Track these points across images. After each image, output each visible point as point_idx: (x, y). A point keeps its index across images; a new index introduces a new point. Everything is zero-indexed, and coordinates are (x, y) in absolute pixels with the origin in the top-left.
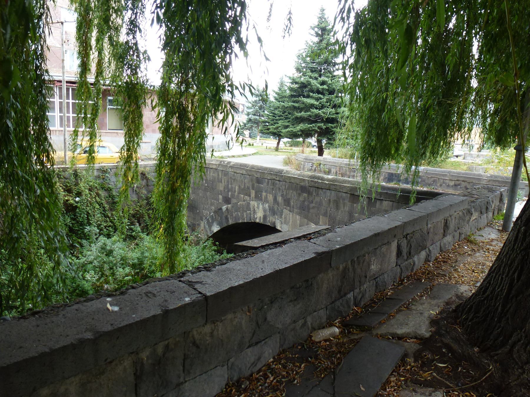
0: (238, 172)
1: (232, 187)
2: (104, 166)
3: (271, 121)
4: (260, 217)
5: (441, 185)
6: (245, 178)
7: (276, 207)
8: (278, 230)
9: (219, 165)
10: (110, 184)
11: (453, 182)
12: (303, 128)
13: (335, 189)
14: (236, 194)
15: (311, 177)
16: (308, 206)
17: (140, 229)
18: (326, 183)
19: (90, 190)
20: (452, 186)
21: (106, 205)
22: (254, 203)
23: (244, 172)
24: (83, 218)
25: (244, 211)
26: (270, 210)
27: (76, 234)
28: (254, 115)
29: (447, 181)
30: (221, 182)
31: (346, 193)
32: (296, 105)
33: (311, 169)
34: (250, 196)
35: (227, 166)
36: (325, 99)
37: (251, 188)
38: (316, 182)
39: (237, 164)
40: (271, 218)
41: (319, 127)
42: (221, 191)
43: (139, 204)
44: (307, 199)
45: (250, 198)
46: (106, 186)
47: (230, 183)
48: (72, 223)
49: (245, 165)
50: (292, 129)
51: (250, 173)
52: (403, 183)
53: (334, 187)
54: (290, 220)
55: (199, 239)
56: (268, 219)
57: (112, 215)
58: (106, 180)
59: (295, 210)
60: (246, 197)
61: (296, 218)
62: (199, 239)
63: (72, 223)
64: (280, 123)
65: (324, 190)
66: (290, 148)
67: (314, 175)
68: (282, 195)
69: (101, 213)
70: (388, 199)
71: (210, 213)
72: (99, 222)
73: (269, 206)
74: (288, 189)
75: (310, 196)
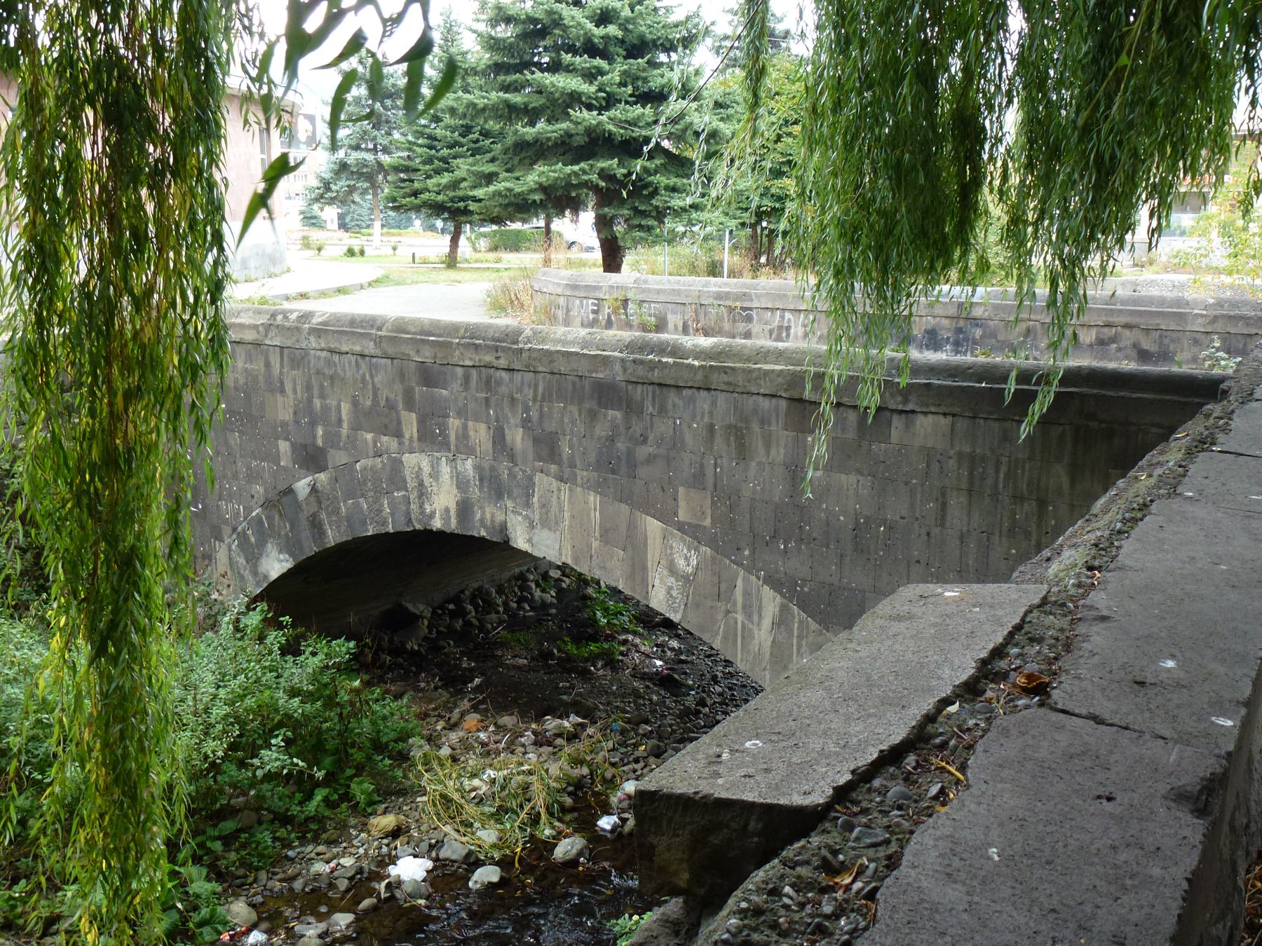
0: (345, 348)
1: (325, 408)
3: (424, 163)
4: (447, 510)
6: (373, 370)
7: (504, 467)
8: (519, 551)
9: (268, 327)
11: (1093, 332)
12: (548, 177)
13: (729, 384)
14: (345, 430)
15: (631, 347)
16: (630, 454)
18: (690, 366)
20: (1091, 345)
22: (416, 462)
23: (370, 348)
25: (379, 492)
26: (481, 480)
28: (357, 148)
30: (283, 391)
32: (516, 98)
34: (398, 434)
35: (298, 329)
36: (616, 73)
37: (401, 406)
38: (652, 366)
39: (336, 319)
40: (488, 510)
41: (603, 174)
42: (284, 424)
44: (622, 429)
47: (316, 392)
49: (373, 322)
50: (508, 185)
52: (920, 347)
53: (725, 378)
54: (561, 510)
55: (215, 609)
56: (478, 516)
59: (581, 475)
60: (385, 439)
61: (586, 503)
62: (215, 609)
64: (463, 167)
65: (686, 392)
66: (491, 256)
67: (643, 338)
68: (526, 423)
70: (933, 409)
71: (248, 510)
73: (477, 468)
74: (547, 397)
75: (634, 418)
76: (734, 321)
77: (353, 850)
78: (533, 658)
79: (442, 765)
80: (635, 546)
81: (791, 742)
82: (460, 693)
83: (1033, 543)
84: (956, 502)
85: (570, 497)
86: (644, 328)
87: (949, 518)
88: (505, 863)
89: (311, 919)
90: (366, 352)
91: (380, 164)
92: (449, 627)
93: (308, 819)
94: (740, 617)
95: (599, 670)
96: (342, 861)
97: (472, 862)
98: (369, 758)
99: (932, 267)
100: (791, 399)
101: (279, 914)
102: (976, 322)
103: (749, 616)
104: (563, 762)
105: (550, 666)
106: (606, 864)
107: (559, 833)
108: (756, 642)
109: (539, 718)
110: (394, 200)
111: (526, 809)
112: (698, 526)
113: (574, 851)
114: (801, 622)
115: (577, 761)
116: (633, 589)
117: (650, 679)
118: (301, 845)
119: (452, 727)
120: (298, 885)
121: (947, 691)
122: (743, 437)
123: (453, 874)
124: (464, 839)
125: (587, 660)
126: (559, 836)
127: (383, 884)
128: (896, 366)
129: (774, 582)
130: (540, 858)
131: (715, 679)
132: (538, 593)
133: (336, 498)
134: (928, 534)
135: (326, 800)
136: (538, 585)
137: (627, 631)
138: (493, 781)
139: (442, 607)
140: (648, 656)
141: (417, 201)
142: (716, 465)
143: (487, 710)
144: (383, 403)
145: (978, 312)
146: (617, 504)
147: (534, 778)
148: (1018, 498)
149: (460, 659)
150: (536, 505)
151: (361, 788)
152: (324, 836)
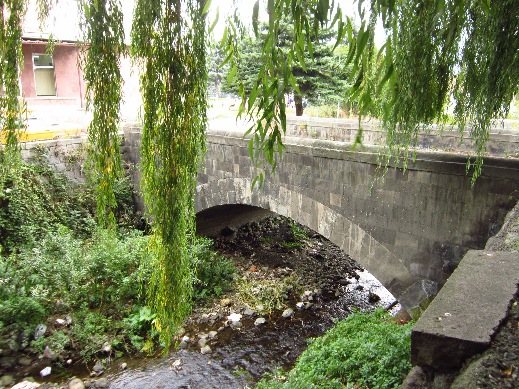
0: (215, 142)
1: (208, 162)
2: (40, 144)
4: (248, 198)
5: (459, 146)
6: (225, 149)
10: (49, 167)
13: (350, 158)
14: (214, 169)
15: (315, 144)
16: (313, 181)
17: (94, 221)
19: (23, 177)
20: (473, 146)
21: (47, 195)
22: (238, 181)
23: (224, 142)
24: (18, 214)
25: (225, 191)
27: (10, 236)
29: (466, 141)
31: (366, 163)
33: (295, 133)
34: (232, 171)
38: (323, 151)
40: (263, 198)
43: (89, 189)
45: (233, 174)
46: (45, 170)
48: (4, 223)
51: (231, 143)
53: (348, 156)
54: (288, 199)
56: (259, 200)
57: (56, 206)
58: (44, 162)
59: (296, 187)
60: (228, 173)
63: (4, 223)
69: (41, 205)
70: (424, 170)
72: (40, 218)
74: (285, 160)
75: (316, 169)
76: (344, 134)
77: (215, 310)
78: (272, 247)
79: (244, 283)
80: (314, 213)
81: (462, 315)
82: (248, 258)
83: (459, 217)
84: (431, 203)
85: (292, 195)
86: (313, 136)
87: (428, 208)
88: (266, 317)
89: (203, 333)
90: (222, 143)
91: (219, 76)
92: (244, 235)
93: (201, 299)
94: (350, 238)
95: (295, 252)
96: (212, 314)
97: (255, 316)
98: (220, 279)
99: (426, 120)
100: (372, 164)
101: (192, 331)
102: (432, 137)
103: (354, 238)
104: (285, 284)
105: (278, 250)
106: (300, 319)
107: (284, 307)
108: (356, 247)
109: (276, 267)
110: (224, 89)
111: (273, 299)
112: (336, 207)
113: (289, 314)
114: (372, 241)
115: (289, 283)
116: (313, 227)
117: (312, 256)
118: (199, 308)
119: (246, 270)
120: (198, 321)
121: (512, 297)
122: (354, 176)
123: (249, 320)
124: (252, 308)
125: (291, 248)
126: (284, 308)
127: (226, 322)
128: (411, 154)
129: (363, 227)
130: (278, 316)
131: (335, 257)
132: (273, 225)
133: (210, 192)
134: (420, 213)
135: (206, 293)
136: (273, 222)
137: (304, 239)
138: (261, 289)
139: (241, 229)
140: (311, 248)
141: (232, 89)
142: (344, 186)
143: (258, 264)
144: (227, 161)
145: (432, 133)
146: (308, 198)
147: (275, 288)
148: (454, 202)
149: (248, 247)
150: (280, 197)
151: (218, 289)
152: (206, 305)
